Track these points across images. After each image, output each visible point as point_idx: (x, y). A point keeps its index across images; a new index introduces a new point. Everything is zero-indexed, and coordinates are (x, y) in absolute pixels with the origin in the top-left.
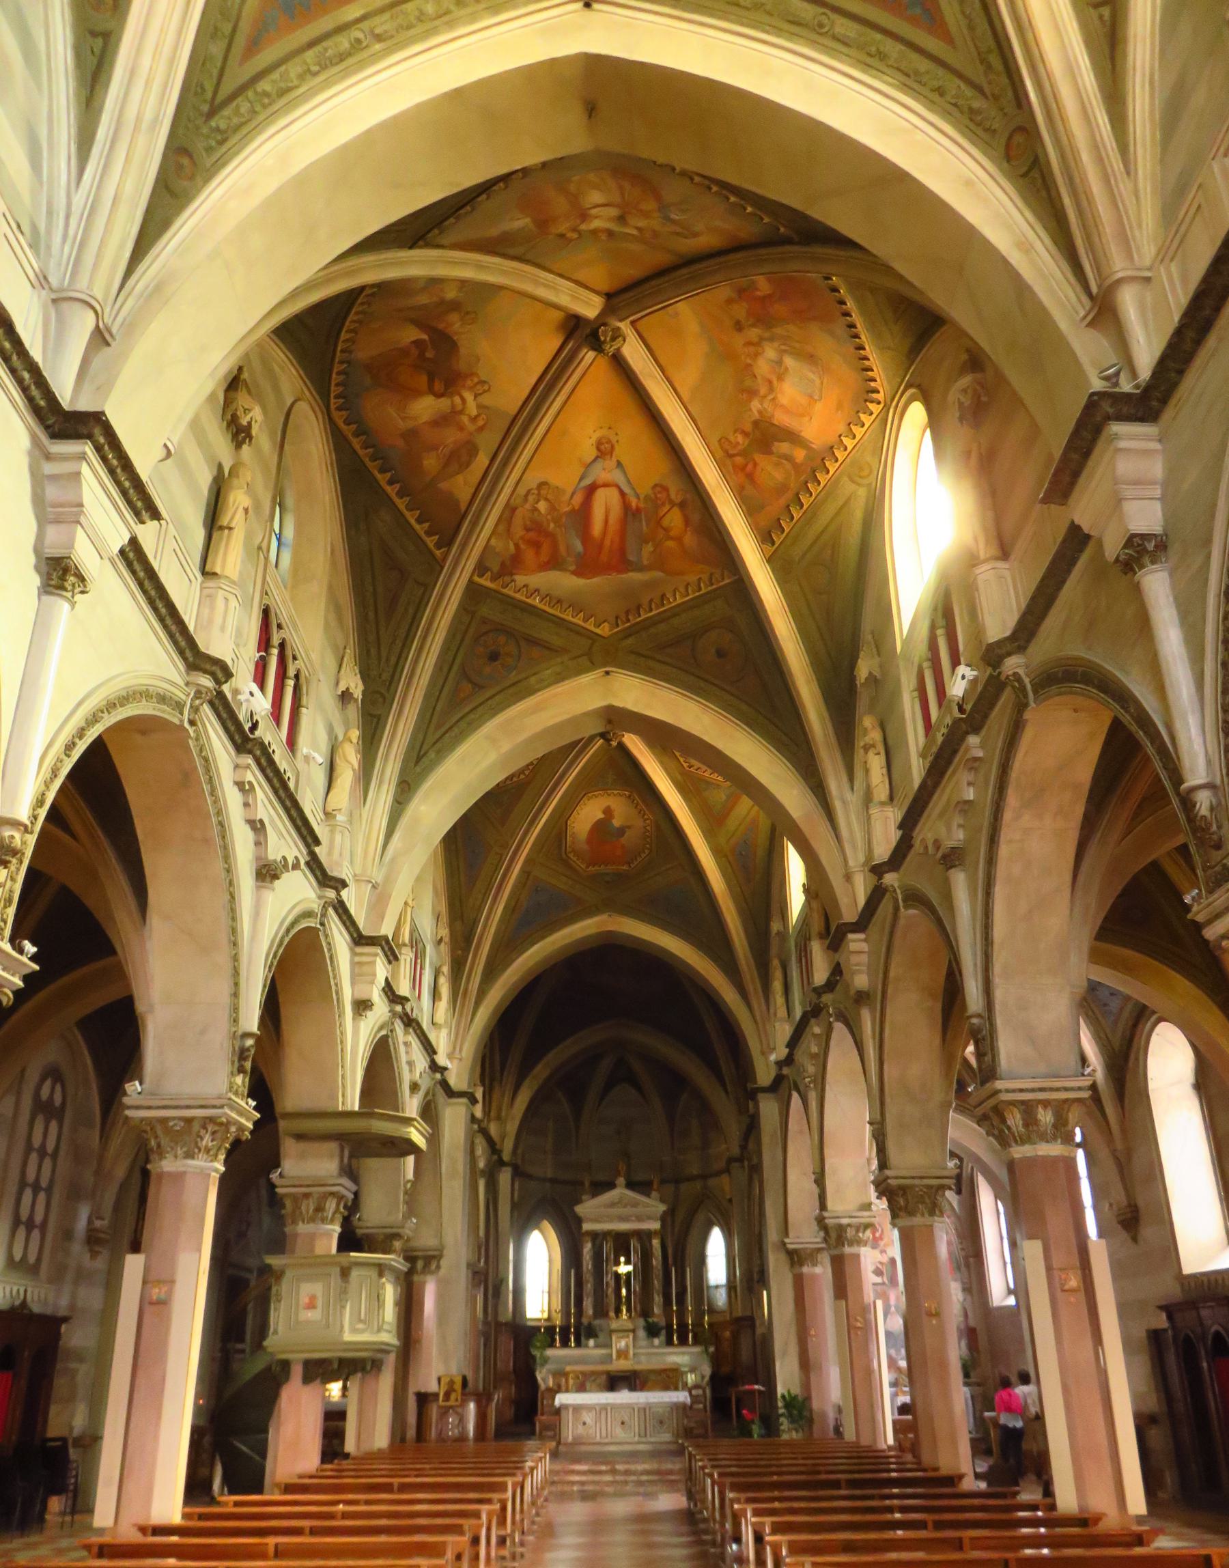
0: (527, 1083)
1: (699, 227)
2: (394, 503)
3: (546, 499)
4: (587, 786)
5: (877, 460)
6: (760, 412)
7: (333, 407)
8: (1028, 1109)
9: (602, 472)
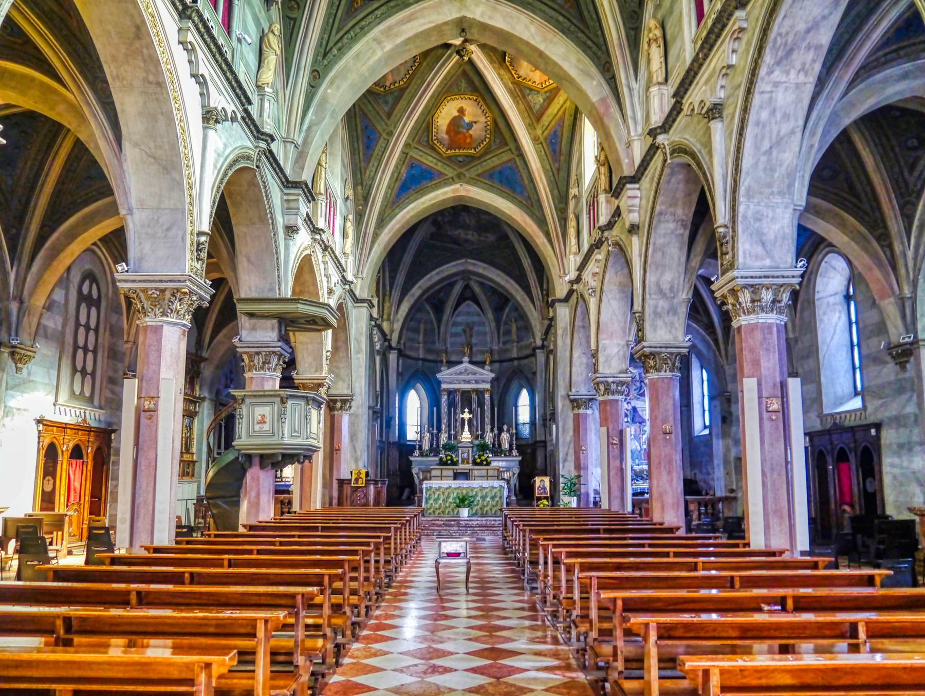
0: (406, 298)
4: (446, 92)
8: (755, 289)
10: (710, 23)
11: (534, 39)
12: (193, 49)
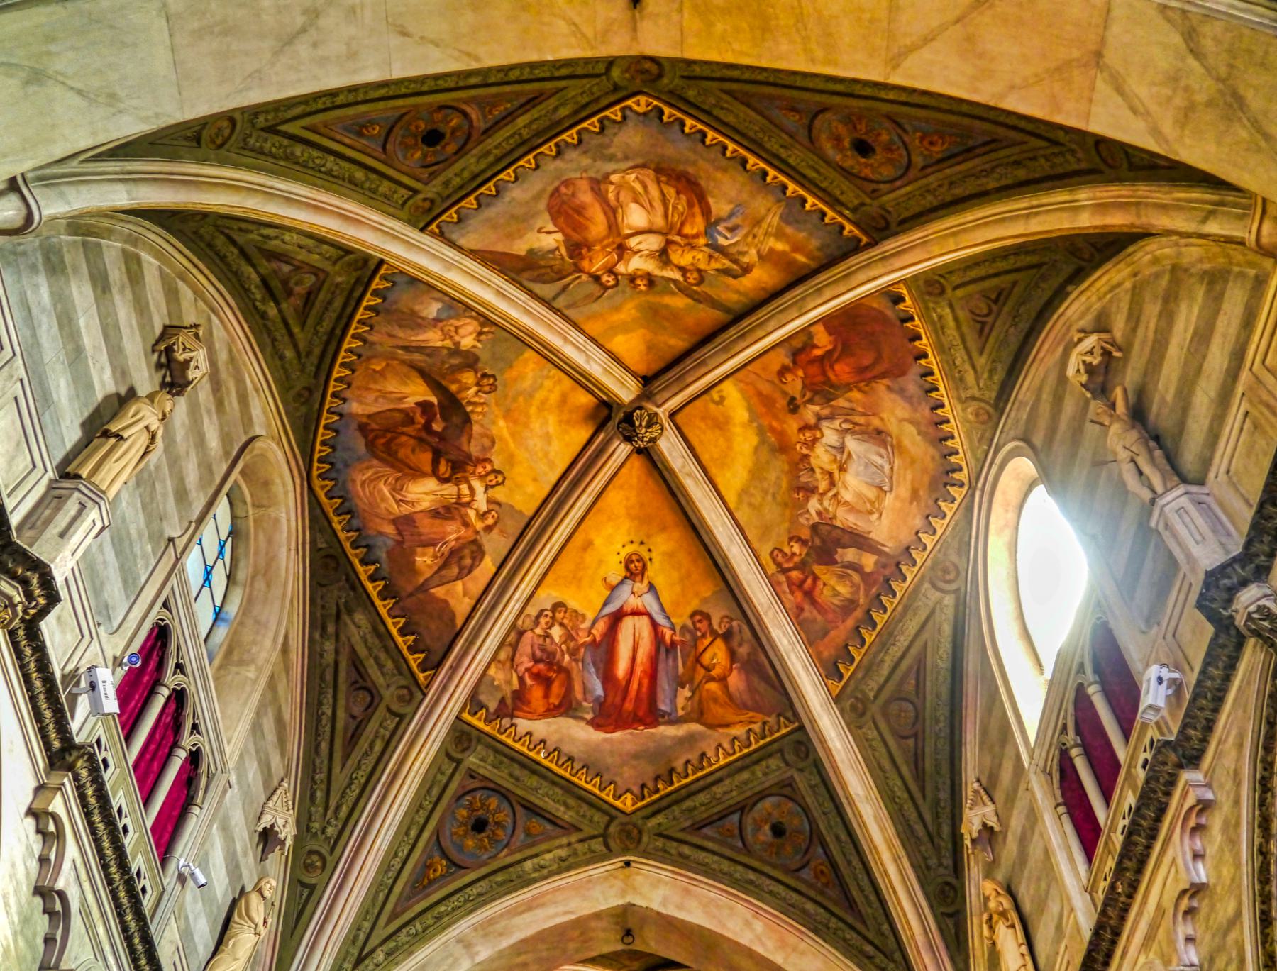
1: (751, 256)
2: (373, 604)
3: (562, 625)
5: (964, 559)
6: (819, 514)
7: (315, 473)
9: (628, 597)
10: (1118, 839)
11: (763, 944)
12: (59, 835)
